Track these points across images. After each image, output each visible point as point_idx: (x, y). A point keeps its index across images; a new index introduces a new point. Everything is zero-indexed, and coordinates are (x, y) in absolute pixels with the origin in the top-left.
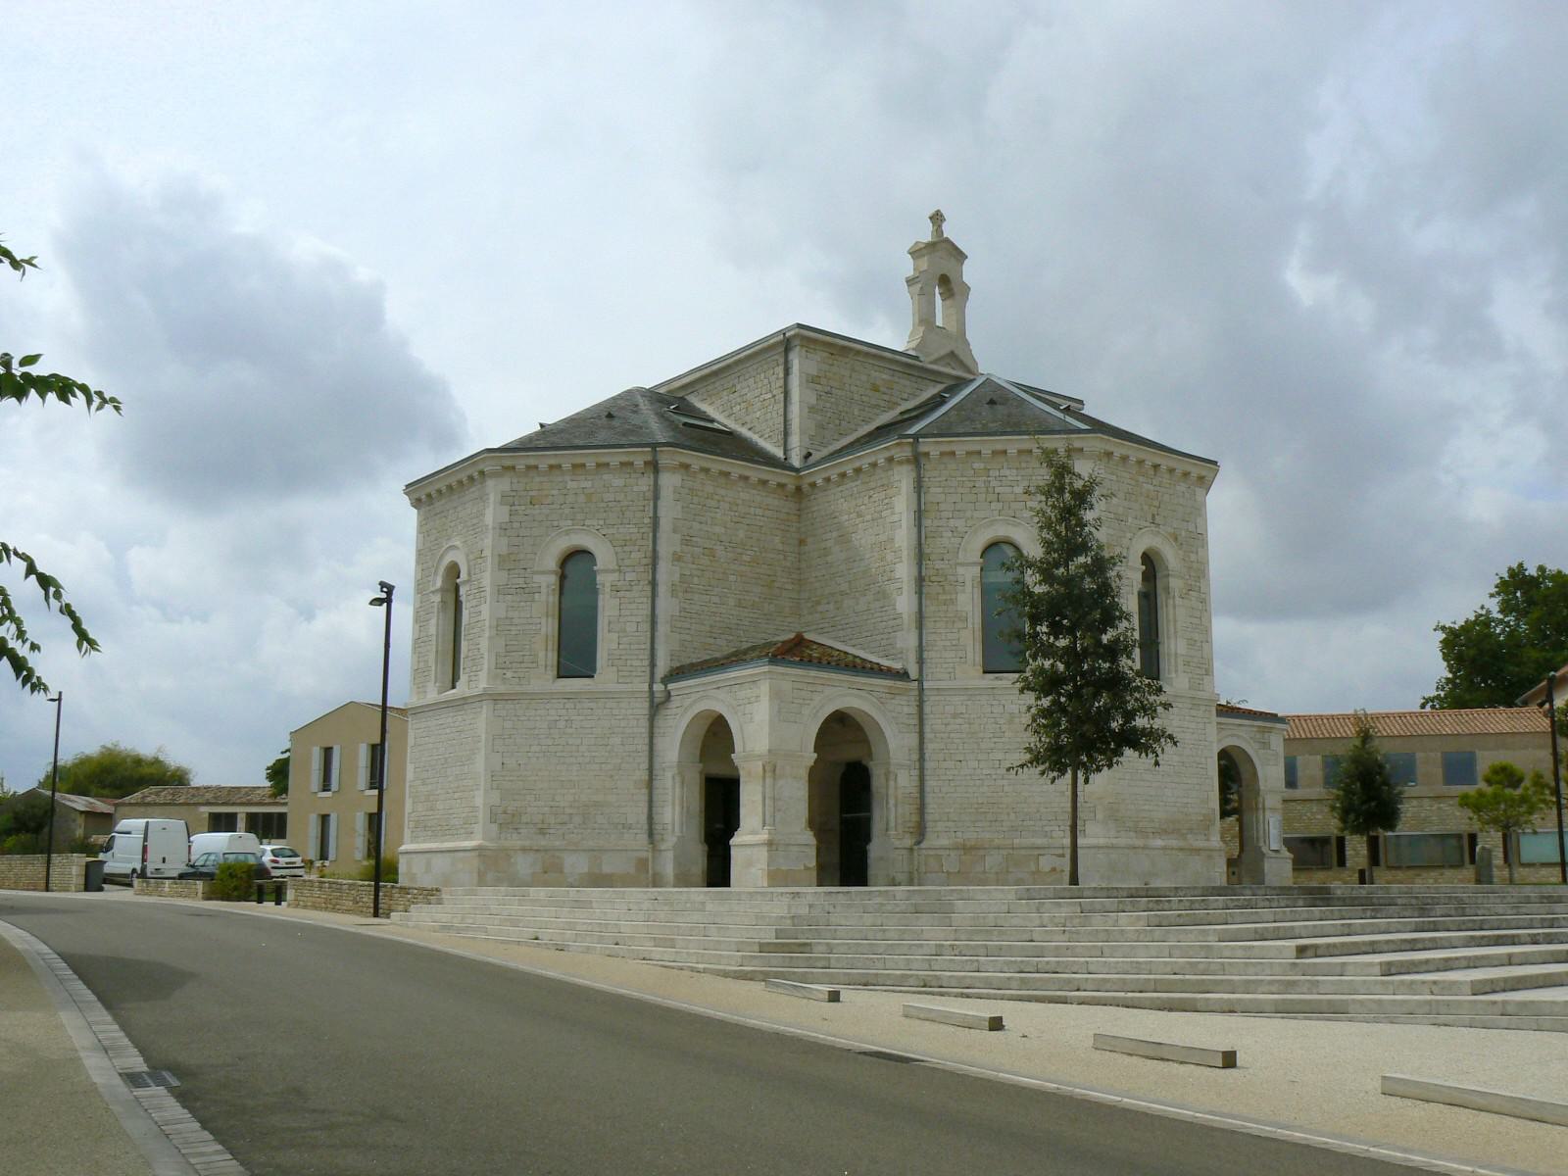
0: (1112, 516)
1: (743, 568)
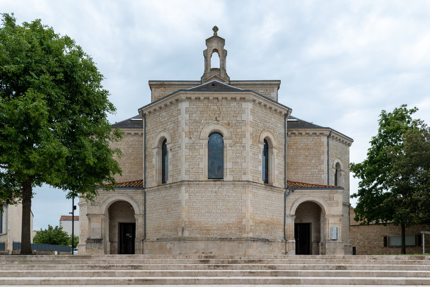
0: (193, 121)
1: (131, 161)
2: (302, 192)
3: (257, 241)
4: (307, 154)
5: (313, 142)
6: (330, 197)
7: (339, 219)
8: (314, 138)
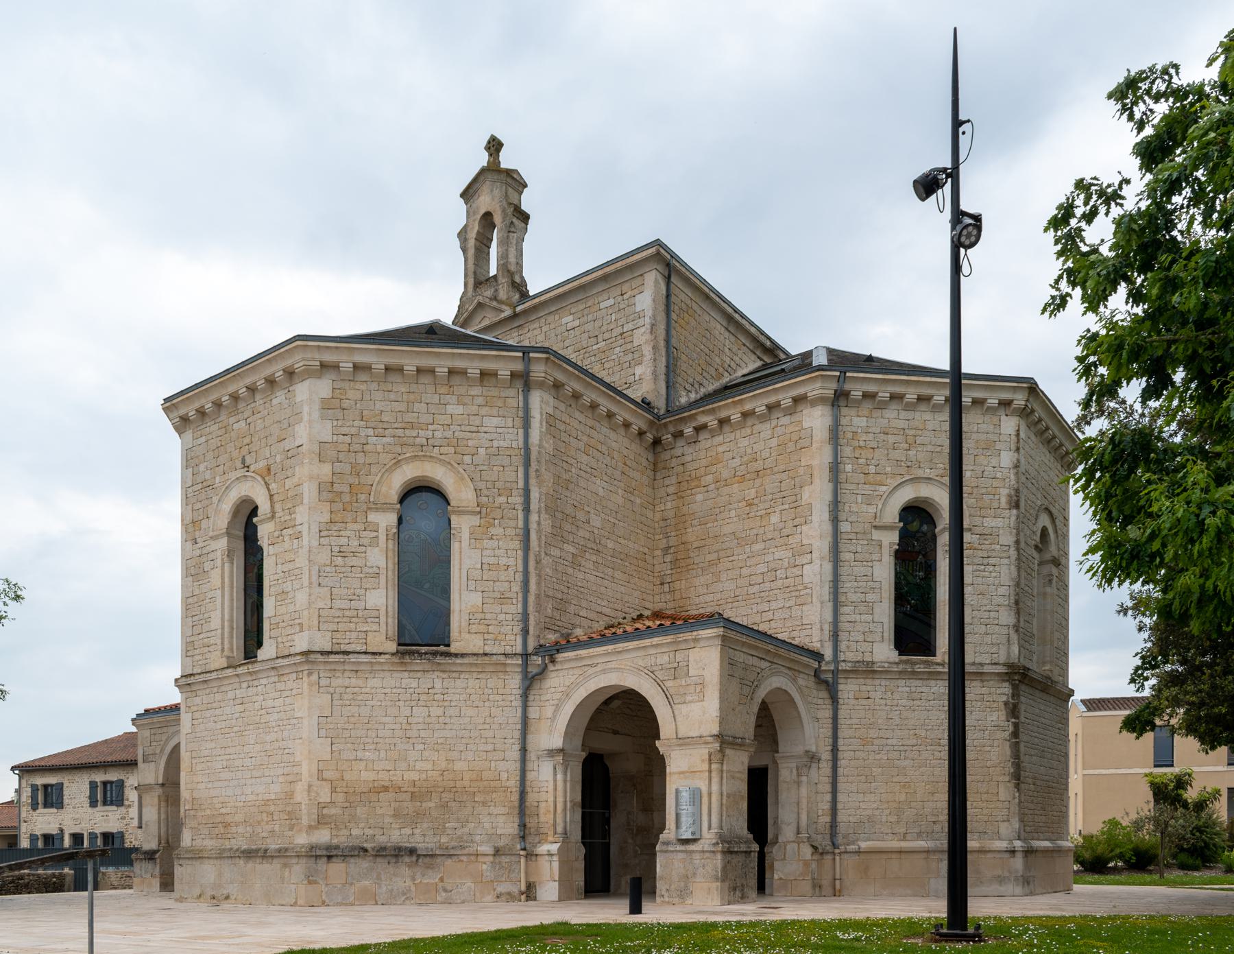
2: (582, 658)
3: (348, 859)
4: (752, 493)
5: (774, 442)
6: (676, 665)
7: (704, 752)
8: (777, 426)
